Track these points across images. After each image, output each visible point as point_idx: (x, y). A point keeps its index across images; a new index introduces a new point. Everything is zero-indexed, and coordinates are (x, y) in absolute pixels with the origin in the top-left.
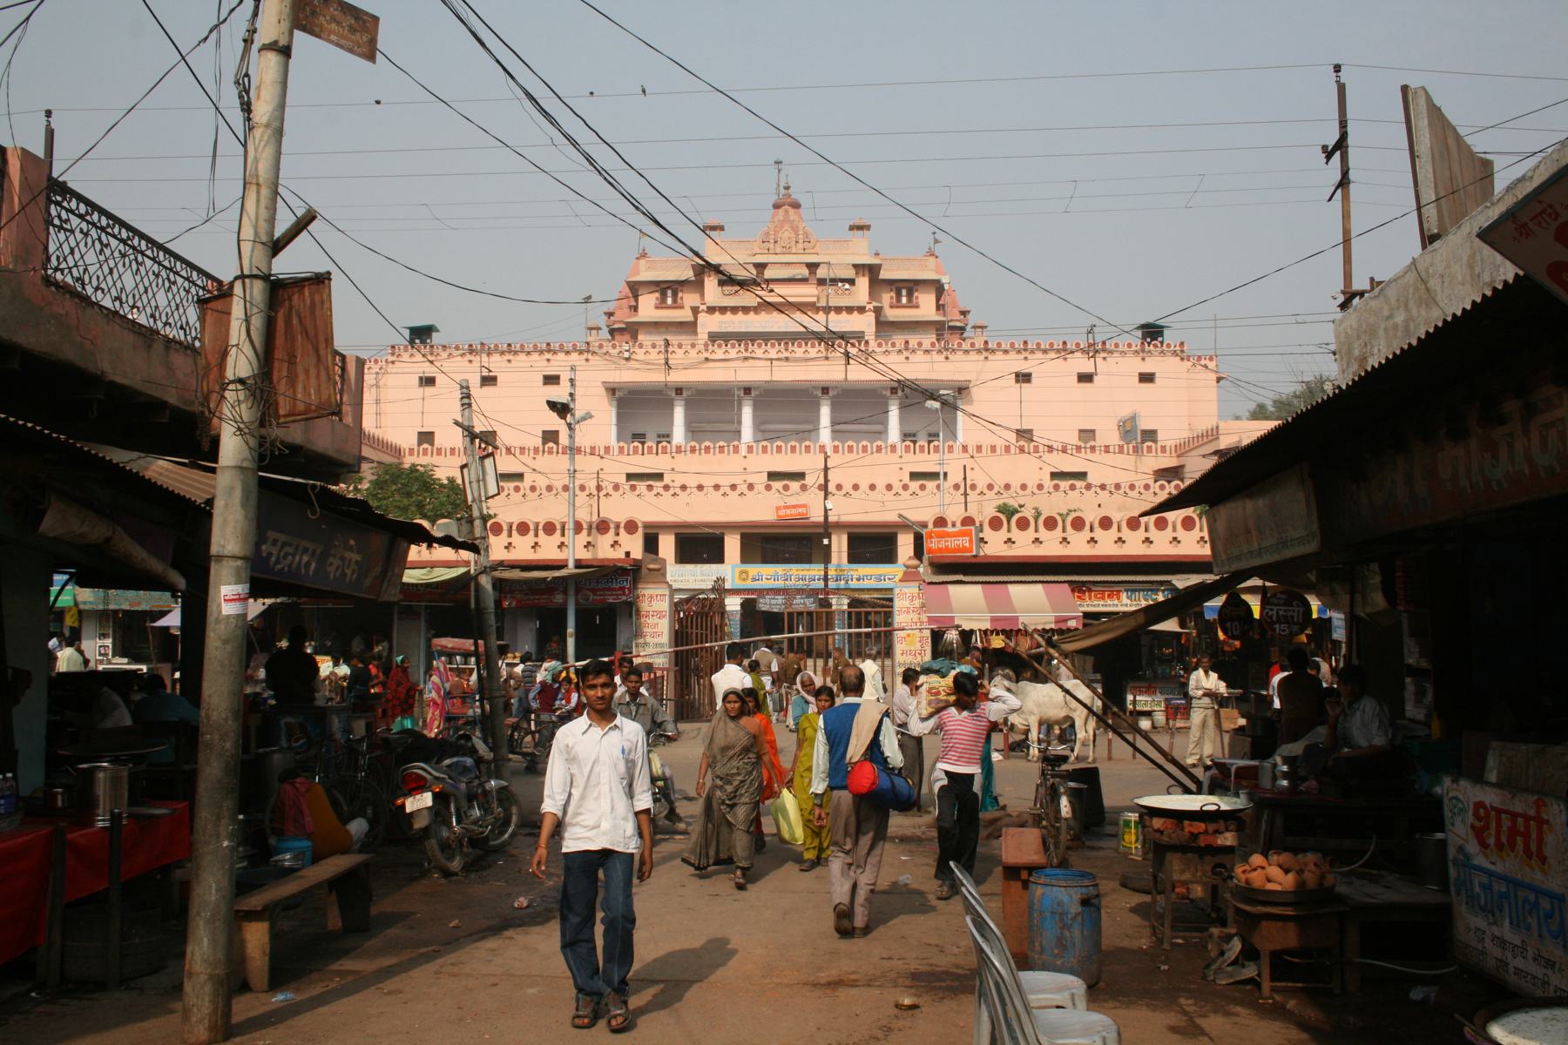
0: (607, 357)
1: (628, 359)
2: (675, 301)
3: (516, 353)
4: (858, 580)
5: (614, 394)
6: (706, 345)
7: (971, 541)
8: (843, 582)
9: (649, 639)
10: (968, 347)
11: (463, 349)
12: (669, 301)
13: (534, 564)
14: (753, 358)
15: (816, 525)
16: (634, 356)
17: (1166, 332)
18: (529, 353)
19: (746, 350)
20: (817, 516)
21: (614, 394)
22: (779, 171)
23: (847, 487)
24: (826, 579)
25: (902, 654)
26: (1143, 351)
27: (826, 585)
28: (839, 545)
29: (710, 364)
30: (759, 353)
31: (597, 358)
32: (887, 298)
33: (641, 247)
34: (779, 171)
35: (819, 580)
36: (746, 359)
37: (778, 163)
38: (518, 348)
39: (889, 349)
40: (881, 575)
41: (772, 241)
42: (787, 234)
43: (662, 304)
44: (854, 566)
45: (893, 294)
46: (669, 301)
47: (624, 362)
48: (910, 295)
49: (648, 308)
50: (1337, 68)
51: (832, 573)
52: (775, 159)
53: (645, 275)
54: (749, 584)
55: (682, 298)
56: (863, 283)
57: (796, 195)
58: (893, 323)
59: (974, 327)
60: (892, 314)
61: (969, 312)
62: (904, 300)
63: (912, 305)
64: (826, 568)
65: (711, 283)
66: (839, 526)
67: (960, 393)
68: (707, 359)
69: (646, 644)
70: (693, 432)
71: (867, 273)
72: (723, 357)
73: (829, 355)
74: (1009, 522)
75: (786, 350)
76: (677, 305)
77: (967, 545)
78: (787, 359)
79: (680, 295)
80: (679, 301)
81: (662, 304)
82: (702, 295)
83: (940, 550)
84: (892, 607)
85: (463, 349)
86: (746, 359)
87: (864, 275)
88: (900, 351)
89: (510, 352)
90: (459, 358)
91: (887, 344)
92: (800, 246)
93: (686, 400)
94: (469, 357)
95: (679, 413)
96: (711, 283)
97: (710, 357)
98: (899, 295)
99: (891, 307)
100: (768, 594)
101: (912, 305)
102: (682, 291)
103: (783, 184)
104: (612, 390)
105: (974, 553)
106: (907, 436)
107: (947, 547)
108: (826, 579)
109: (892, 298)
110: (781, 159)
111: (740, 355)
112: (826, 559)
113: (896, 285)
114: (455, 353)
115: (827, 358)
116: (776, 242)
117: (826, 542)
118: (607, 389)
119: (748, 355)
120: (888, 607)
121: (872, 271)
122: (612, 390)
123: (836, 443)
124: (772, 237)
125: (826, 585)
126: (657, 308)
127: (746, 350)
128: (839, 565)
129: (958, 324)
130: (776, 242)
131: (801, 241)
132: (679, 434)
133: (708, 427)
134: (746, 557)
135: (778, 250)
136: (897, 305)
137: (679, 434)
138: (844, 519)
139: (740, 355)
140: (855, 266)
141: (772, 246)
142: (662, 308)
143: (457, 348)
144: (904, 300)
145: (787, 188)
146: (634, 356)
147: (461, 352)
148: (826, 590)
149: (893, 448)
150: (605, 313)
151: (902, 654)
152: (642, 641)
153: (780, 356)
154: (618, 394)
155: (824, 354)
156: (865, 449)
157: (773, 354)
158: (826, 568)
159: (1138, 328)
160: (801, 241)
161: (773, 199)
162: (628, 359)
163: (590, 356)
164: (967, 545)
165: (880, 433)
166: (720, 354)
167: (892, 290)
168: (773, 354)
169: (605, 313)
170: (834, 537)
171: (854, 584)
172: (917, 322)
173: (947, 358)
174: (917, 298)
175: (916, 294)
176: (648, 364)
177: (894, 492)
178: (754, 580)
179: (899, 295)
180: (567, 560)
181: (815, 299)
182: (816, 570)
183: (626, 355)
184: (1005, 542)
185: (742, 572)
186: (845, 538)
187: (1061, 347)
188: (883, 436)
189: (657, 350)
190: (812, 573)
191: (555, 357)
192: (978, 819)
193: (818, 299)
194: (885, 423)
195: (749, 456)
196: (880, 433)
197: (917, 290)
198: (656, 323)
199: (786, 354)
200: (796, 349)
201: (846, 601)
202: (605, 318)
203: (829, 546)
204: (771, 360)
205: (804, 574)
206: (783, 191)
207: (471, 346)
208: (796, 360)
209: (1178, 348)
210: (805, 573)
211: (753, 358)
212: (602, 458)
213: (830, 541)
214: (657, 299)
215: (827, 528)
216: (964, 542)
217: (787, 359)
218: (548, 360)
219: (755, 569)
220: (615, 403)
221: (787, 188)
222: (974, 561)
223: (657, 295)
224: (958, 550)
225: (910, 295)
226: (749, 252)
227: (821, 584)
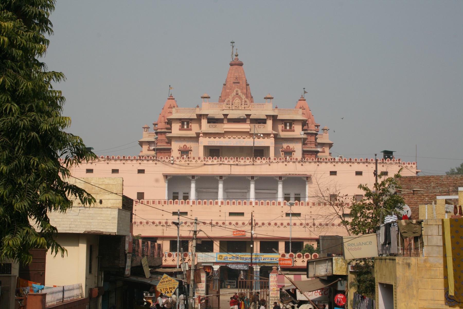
0: (164, 163)
1: (172, 164)
2: (188, 127)
3: (127, 160)
4: (264, 259)
5: (167, 178)
6: (204, 158)
7: (291, 262)
8: (258, 260)
9: (199, 289)
10: (311, 161)
11: (105, 158)
12: (185, 127)
13: (166, 266)
14: (224, 164)
15: (248, 238)
16: (175, 162)
17: (393, 153)
18: (132, 160)
19: (221, 161)
20: (248, 235)
21: (167, 178)
22: (233, 47)
23: (260, 224)
24: (251, 259)
25: (272, 294)
26: (383, 163)
27: (251, 261)
28: (257, 246)
29: (206, 166)
30: (226, 162)
31: (160, 163)
32: (280, 127)
33: (170, 94)
34: (233, 47)
35: (249, 259)
36: (221, 164)
37: (233, 43)
38: (128, 158)
39: (279, 161)
40: (272, 258)
41: (231, 104)
42: (237, 101)
43: (182, 128)
44: (262, 254)
45: (283, 125)
46: (185, 127)
47: (171, 165)
48: (290, 126)
49: (176, 130)
50: (376, 155)
51: (254, 257)
52: (231, 41)
53: (175, 115)
54: (222, 261)
55: (191, 126)
56: (270, 123)
57: (241, 59)
58: (283, 138)
59: (323, 130)
60: (283, 134)
61: (319, 126)
62: (288, 128)
63: (291, 130)
64: (252, 256)
65: (204, 122)
66: (257, 239)
67: (307, 179)
68: (205, 164)
69: (198, 290)
70: (198, 192)
71: (271, 119)
72: (211, 163)
73: (254, 163)
74: (303, 256)
75: (237, 161)
76: (189, 129)
77: (290, 263)
78: (237, 165)
79: (190, 124)
80: (190, 127)
81: (182, 128)
82: (200, 127)
83: (283, 264)
84: (269, 280)
85: (105, 158)
86: (221, 164)
87: (270, 120)
88: (283, 162)
89: (124, 160)
90: (103, 162)
91: (278, 159)
92: (243, 106)
93: (196, 180)
94: (107, 161)
95: (193, 186)
96: (204, 122)
97: (206, 163)
98: (286, 126)
99: (282, 131)
100: (229, 264)
101: (291, 130)
102: (191, 123)
103: (235, 53)
104: (166, 176)
105: (292, 265)
106: (287, 198)
107: (285, 263)
108: (251, 259)
109: (282, 127)
110: (234, 41)
111: (218, 163)
112: (252, 251)
113: (285, 122)
114: (101, 159)
115: (253, 164)
116: (232, 104)
117: (252, 246)
118: (164, 176)
119: (221, 163)
120: (267, 280)
121: (274, 118)
122: (166, 176)
123: (257, 201)
124: (231, 102)
125: (251, 261)
126: (180, 130)
127: (221, 161)
128: (256, 254)
129: (314, 132)
130: (232, 104)
131: (243, 104)
132: (193, 195)
133: (204, 190)
134: (222, 250)
135: (234, 108)
136: (285, 130)
137: (193, 195)
138: (259, 236)
139: (218, 163)
140: (266, 116)
141: (231, 106)
142: (182, 130)
143: (102, 158)
144: (288, 128)
145: (237, 56)
146: (175, 162)
147: (104, 159)
148: (252, 263)
149: (279, 203)
150: (153, 124)
151: (272, 294)
152: (197, 289)
153: (234, 163)
154: (168, 178)
155: (252, 163)
156: (268, 204)
157: (231, 162)
158: (252, 256)
159: (382, 152)
160: (243, 104)
161: (230, 60)
162: (172, 164)
163: (157, 162)
164: (290, 263)
165: (275, 194)
166: (210, 162)
167: (283, 124)
168: (231, 162)
169: (153, 124)
170: (255, 243)
171: (262, 261)
172: (294, 138)
173: (302, 165)
174: (294, 127)
175: (293, 125)
176: (180, 165)
177: (277, 226)
178: (224, 259)
179: (286, 126)
180: (177, 265)
181: (249, 130)
182: (247, 256)
183: (172, 162)
184: (302, 262)
185: (220, 256)
186: (259, 243)
187: (349, 161)
188: (276, 195)
189: (184, 160)
190: (246, 256)
191: (143, 162)
192: (234, 305)
193: (250, 129)
194: (277, 190)
195: (222, 206)
196: (275, 194)
197: (293, 124)
198: (180, 137)
199: (237, 163)
200: (241, 161)
201: (259, 267)
202: (153, 126)
203: (253, 248)
204: (231, 165)
205: (245, 256)
206: (234, 57)
207: (108, 157)
208: (241, 165)
209: (397, 161)
210: (244, 256)
211: (224, 164)
212: (163, 206)
213: (253, 246)
214: (180, 126)
215: (252, 240)
216: (289, 262)
217: (237, 165)
218: (140, 163)
219: (225, 255)
220: (167, 181)
221: (237, 56)
222: (292, 267)
223: (180, 124)
224: (288, 264)
225: (290, 126)
226: (221, 109)
227: (250, 261)
